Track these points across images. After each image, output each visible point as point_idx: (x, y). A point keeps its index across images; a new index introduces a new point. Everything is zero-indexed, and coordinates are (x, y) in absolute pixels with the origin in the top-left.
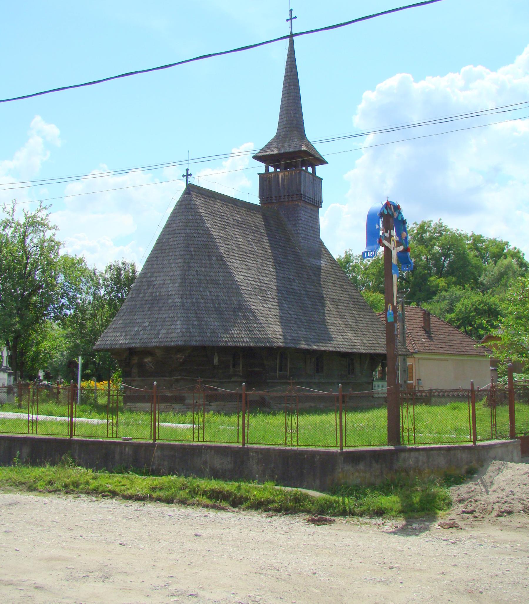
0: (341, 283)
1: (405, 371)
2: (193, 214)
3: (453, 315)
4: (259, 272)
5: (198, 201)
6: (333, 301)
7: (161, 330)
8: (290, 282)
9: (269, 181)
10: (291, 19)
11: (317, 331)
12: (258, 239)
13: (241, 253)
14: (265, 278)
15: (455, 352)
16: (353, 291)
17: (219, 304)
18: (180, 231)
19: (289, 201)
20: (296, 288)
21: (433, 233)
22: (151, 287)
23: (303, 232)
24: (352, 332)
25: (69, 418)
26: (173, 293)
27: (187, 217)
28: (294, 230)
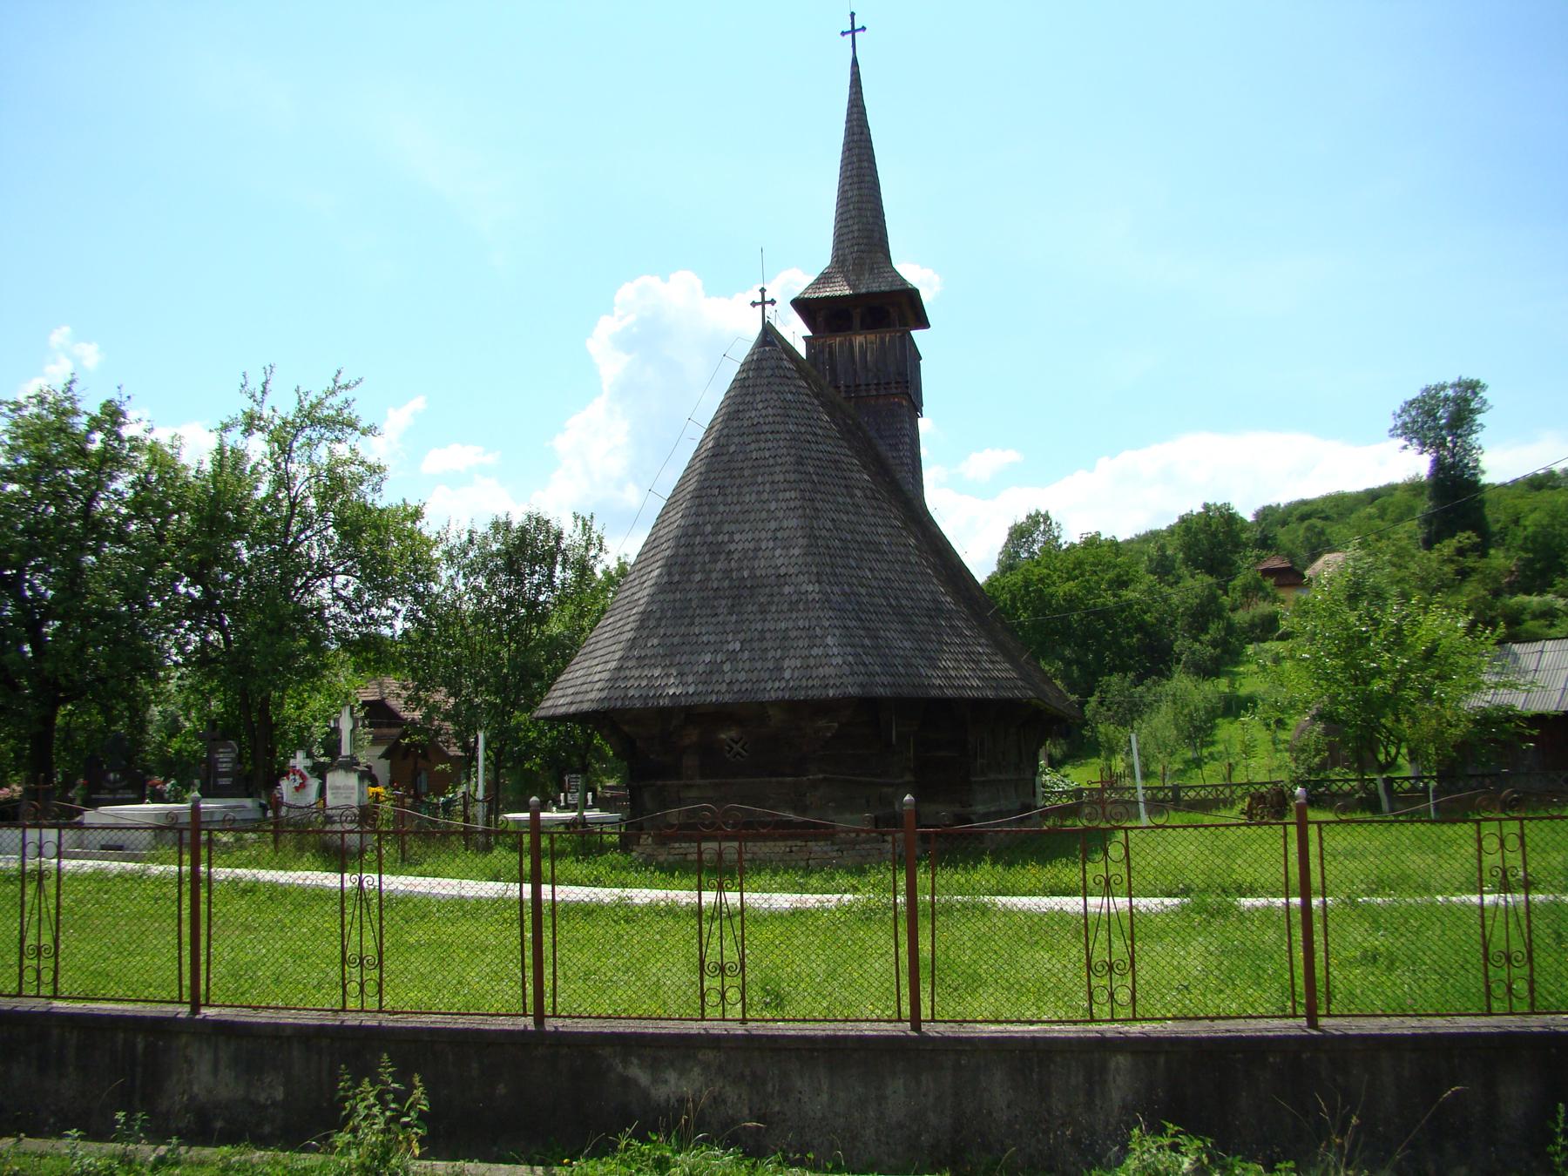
7: (782, 658)
9: (831, 353)
10: (853, 31)
17: (896, 598)
18: (772, 428)
19: (878, 397)
22: (723, 557)
25: (527, 888)
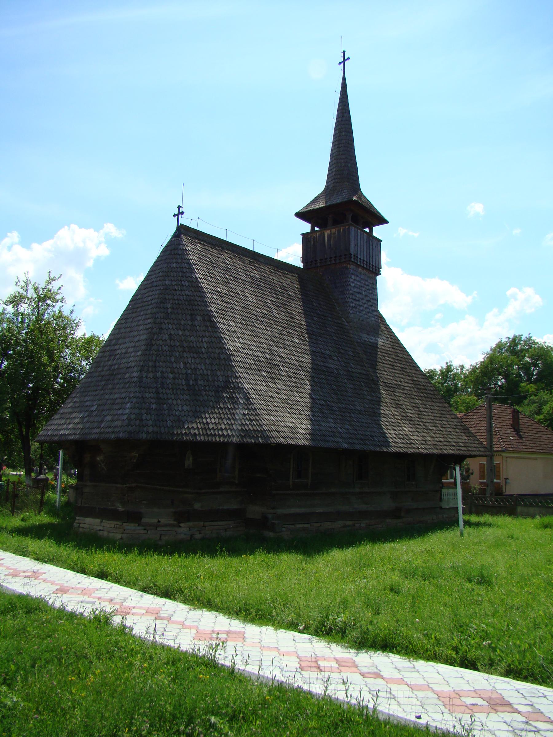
0: (402, 366)
1: (491, 470)
2: (180, 261)
3: (541, 417)
4: (273, 341)
5: (192, 250)
6: (388, 386)
8: (325, 358)
9: (314, 242)
11: (353, 423)
12: (282, 302)
13: (246, 315)
14: (281, 350)
15: (544, 451)
16: (420, 376)
20: (332, 366)
21: (524, 346)
23: (353, 301)
24: (411, 426)
26: (133, 364)
27: (169, 265)
28: (342, 299)
